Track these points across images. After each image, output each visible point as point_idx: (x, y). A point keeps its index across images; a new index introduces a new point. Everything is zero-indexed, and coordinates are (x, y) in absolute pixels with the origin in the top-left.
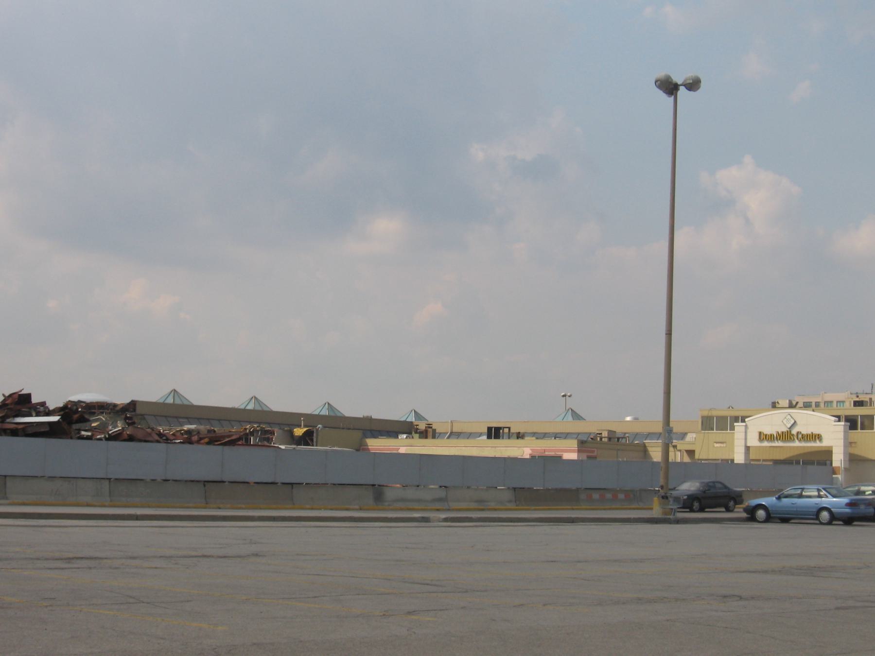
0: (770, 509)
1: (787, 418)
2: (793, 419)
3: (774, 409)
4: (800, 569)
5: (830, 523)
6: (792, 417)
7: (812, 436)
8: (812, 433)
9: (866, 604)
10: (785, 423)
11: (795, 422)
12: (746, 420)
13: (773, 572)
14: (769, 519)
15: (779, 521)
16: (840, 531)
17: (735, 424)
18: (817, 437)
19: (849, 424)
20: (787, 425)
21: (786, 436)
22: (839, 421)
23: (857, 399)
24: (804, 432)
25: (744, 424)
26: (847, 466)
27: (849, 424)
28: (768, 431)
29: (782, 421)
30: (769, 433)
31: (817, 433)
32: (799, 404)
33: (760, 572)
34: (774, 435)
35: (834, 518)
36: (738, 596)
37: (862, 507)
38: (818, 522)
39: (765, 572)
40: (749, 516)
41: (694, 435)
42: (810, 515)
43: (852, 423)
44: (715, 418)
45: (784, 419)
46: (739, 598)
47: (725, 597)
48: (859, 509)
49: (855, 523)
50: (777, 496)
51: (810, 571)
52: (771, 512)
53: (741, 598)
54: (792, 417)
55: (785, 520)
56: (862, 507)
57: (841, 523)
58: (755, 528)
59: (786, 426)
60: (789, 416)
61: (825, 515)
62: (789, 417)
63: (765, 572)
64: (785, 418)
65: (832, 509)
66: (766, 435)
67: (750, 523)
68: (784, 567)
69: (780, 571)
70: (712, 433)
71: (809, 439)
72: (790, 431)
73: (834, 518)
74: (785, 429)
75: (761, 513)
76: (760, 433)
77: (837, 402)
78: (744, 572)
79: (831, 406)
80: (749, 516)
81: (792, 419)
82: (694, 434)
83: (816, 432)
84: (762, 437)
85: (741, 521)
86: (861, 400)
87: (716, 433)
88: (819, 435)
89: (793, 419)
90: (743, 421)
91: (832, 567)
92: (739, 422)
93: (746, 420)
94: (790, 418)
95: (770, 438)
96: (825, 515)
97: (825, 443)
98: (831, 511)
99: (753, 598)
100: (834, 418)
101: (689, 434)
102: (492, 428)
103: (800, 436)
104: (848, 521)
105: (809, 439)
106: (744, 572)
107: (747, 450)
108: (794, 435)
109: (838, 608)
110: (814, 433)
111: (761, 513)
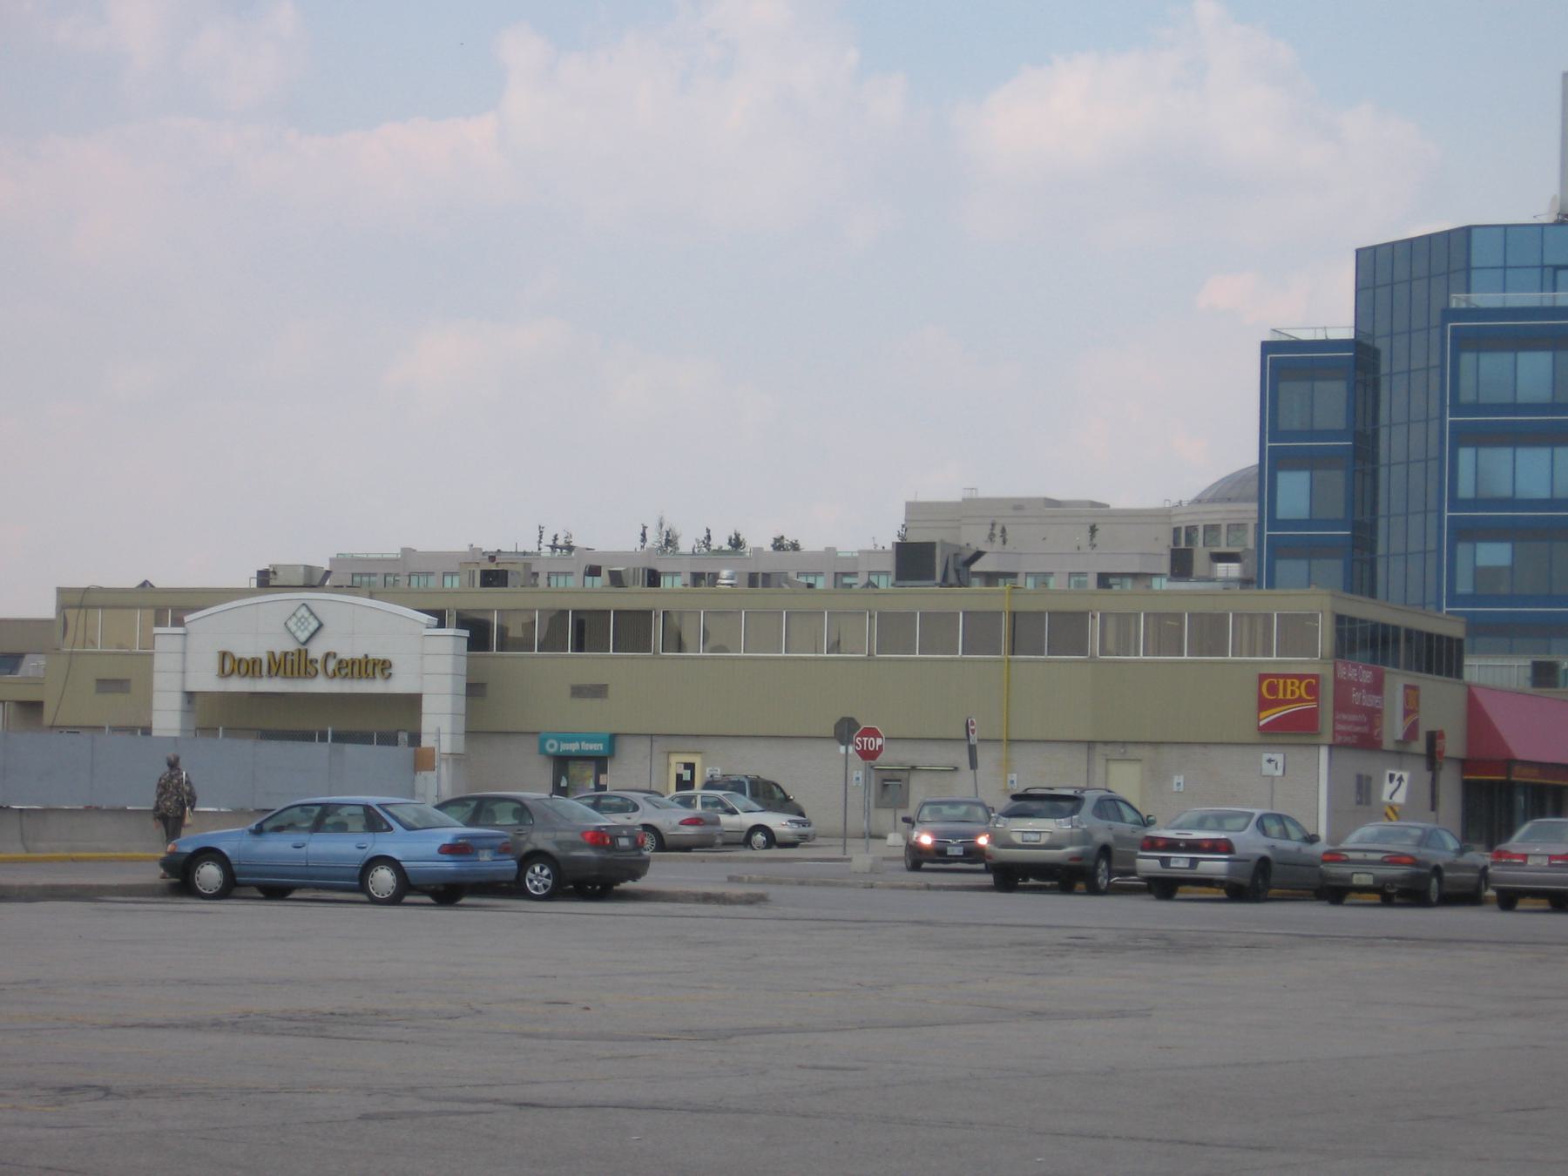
0: (233, 861)
1: (299, 615)
2: (316, 618)
3: (263, 589)
4: (290, 1019)
5: (395, 900)
6: (312, 613)
7: (367, 663)
8: (366, 656)
9: (456, 1106)
10: (294, 628)
11: (321, 626)
12: (187, 619)
13: (217, 1025)
14: (230, 888)
15: (262, 896)
16: (424, 919)
17: (157, 630)
18: (378, 670)
19: (466, 633)
20: (298, 634)
21: (296, 663)
22: (441, 625)
23: (493, 567)
24: (346, 653)
25: (180, 630)
26: (461, 747)
27: (466, 633)
28: (246, 649)
29: (286, 624)
30: (248, 656)
31: (381, 657)
32: (983, 559)
33: (176, 1026)
34: (261, 661)
35: (408, 887)
36: (100, 1088)
37: (485, 856)
38: (363, 897)
39: (195, 1026)
40: (177, 880)
41: (41, 661)
42: (344, 878)
43: (478, 634)
44: (496, 612)
45: (290, 618)
46: (101, 1094)
47: (66, 1089)
48: (478, 860)
49: (465, 901)
50: (253, 826)
51: (318, 1025)
52: (235, 869)
53: (107, 1092)
54: (312, 613)
55: (276, 892)
56: (485, 856)
57: (428, 899)
58: (188, 912)
59: (296, 638)
60: (303, 610)
61: (384, 879)
62: (303, 611)
63: (195, 1026)
64: (294, 614)
65: (402, 863)
66: (240, 660)
67: (178, 900)
68: (247, 1015)
69: (234, 1024)
70: (563, 657)
71: (296, 672)
72: (306, 651)
73: (408, 887)
74: (291, 646)
75: (209, 874)
76: (224, 655)
77: (444, 574)
78: (133, 1026)
79: (536, 585)
80: (177, 880)
81: (311, 619)
82: (43, 656)
83: (377, 653)
84: (231, 664)
85: (155, 895)
86: (500, 568)
87: (964, 661)
88: (384, 662)
89: (316, 618)
90: (178, 622)
91: (377, 1013)
92: (167, 626)
93: (187, 619)
94: (307, 614)
95: (250, 668)
96: (384, 879)
97: (400, 684)
98: (401, 866)
99: (140, 1092)
100: (425, 618)
101: (27, 657)
102: (564, 613)
103: (332, 665)
104: (447, 893)
105: (296, 672)
106: (133, 1026)
107: (189, 702)
108: (317, 661)
109: (365, 1117)
110: (370, 657)
111: (209, 874)
